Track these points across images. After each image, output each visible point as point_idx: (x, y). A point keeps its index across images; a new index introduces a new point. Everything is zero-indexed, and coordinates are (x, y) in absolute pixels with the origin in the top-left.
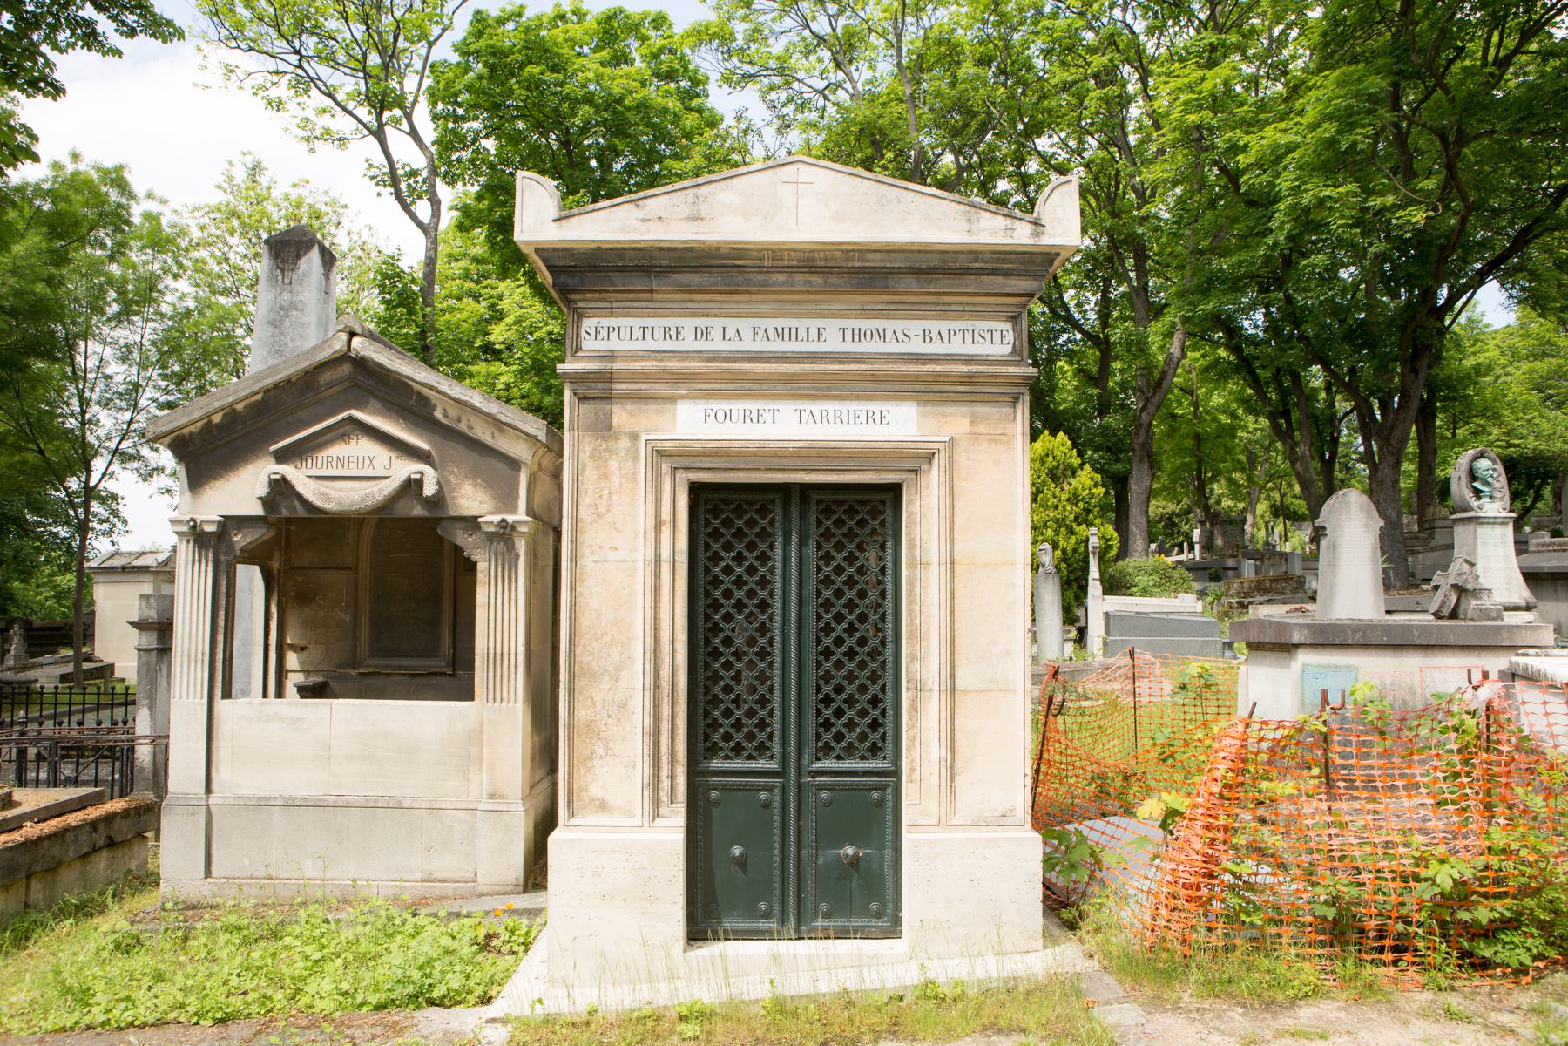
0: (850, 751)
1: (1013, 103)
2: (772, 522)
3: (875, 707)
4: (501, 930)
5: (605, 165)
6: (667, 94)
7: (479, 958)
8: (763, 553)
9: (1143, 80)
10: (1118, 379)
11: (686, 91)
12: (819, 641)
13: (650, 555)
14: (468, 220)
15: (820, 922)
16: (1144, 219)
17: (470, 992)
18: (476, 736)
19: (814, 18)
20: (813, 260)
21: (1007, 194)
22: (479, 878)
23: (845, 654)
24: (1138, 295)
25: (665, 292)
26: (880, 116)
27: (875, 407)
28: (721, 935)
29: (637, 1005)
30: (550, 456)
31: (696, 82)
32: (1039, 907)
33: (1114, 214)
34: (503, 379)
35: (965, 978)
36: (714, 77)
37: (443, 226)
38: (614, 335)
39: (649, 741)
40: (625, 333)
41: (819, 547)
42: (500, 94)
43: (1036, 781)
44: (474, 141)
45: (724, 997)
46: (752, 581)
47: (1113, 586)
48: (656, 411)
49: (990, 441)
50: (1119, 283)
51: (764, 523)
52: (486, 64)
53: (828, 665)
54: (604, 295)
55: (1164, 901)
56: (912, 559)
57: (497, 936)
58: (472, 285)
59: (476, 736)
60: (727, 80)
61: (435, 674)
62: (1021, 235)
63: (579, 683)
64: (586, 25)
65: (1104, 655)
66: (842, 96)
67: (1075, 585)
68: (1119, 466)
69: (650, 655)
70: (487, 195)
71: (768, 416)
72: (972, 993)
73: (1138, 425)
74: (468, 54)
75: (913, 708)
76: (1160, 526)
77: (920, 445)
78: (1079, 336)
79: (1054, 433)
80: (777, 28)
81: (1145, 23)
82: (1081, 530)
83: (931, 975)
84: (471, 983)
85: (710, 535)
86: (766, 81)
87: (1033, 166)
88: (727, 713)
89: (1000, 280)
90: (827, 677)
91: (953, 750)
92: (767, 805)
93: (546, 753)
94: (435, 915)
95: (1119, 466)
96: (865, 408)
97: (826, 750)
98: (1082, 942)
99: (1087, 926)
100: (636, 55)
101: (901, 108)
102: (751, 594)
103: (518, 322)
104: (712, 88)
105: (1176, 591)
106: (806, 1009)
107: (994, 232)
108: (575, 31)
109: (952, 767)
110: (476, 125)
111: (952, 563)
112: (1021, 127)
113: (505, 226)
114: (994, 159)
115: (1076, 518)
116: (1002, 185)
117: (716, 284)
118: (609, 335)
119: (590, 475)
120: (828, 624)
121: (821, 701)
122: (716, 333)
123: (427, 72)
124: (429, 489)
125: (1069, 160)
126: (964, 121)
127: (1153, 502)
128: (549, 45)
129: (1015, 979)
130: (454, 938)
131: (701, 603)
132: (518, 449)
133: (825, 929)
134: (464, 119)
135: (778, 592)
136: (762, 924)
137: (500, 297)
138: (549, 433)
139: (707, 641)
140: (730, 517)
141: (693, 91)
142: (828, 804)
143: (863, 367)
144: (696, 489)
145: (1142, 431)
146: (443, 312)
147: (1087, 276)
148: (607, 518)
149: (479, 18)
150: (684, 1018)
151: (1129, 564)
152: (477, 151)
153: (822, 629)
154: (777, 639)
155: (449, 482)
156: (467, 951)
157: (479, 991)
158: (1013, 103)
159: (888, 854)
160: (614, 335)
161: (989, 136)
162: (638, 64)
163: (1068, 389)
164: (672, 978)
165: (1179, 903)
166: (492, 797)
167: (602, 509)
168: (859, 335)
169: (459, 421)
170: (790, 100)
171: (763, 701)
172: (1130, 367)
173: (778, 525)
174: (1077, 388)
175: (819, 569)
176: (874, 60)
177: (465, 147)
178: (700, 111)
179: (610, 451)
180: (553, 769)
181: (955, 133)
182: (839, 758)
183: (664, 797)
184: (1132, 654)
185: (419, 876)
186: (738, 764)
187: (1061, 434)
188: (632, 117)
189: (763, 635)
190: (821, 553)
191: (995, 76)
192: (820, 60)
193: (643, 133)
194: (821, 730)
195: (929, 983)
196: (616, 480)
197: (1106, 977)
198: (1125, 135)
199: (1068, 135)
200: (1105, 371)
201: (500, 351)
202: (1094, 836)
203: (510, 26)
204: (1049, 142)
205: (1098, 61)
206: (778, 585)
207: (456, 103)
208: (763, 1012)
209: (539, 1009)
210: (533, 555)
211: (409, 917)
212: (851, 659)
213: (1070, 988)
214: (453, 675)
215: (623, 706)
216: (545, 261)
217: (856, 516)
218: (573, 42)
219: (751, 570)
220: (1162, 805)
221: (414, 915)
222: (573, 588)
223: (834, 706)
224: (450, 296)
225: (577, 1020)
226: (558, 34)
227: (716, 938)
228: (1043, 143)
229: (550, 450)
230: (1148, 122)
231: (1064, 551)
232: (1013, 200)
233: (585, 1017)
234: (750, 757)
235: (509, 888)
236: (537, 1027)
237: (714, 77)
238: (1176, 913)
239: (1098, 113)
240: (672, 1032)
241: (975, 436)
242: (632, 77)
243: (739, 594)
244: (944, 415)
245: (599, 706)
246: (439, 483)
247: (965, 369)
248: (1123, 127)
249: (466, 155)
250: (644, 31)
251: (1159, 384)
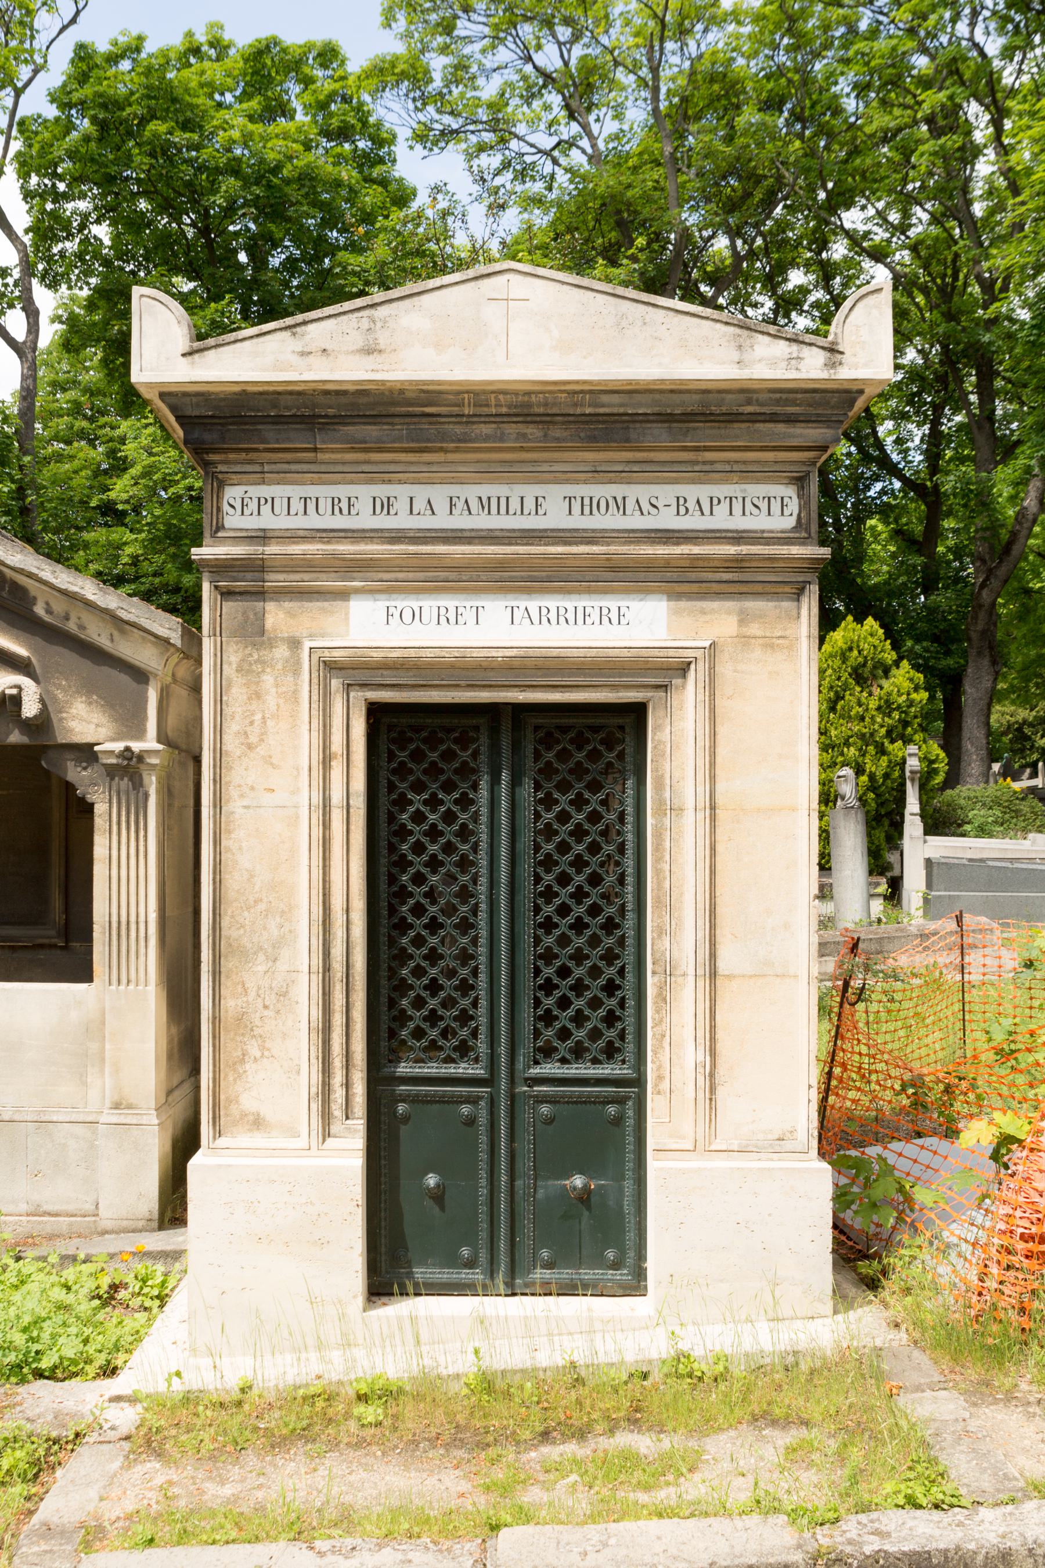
0: (578, 1053)
1: (814, 163)
2: (475, 755)
3: (611, 995)
4: (129, 1279)
5: (259, 260)
6: (339, 160)
7: (101, 1316)
8: (464, 795)
9: (997, 123)
10: (951, 543)
11: (365, 155)
12: (537, 910)
13: (317, 799)
14: (72, 343)
15: (539, 1274)
16: (994, 322)
17: (88, 1361)
18: (96, 1028)
19: (539, 47)
20: (530, 405)
21: (804, 291)
22: (103, 1212)
23: (571, 927)
24: (980, 428)
25: (333, 451)
26: (629, 186)
27: (612, 603)
28: (411, 1290)
29: (301, 1380)
30: (186, 664)
31: (379, 142)
32: (827, 1259)
33: (951, 316)
34: (129, 550)
35: (728, 1351)
36: (403, 134)
37: (45, 340)
38: (266, 509)
39: (317, 1040)
40: (280, 506)
41: (538, 787)
42: (115, 162)
43: (826, 1091)
44: (82, 227)
45: (415, 1370)
46: (449, 832)
47: (938, 823)
48: (323, 609)
49: (765, 646)
50: (956, 411)
51: (465, 755)
52: (94, 120)
53: (549, 941)
54: (252, 456)
55: (996, 1257)
56: (660, 802)
57: (125, 1286)
58: (85, 424)
59: (96, 1028)
60: (421, 137)
61: (42, 946)
62: (812, 367)
63: (228, 964)
64: (228, 63)
65: (926, 914)
66: (577, 158)
67: (886, 822)
68: (950, 662)
69: (317, 929)
70: (102, 303)
71: (469, 616)
72: (738, 1371)
73: (977, 606)
74: (70, 105)
75: (661, 998)
76: (1006, 739)
77: (671, 653)
78: (897, 485)
79: (860, 620)
80: (489, 62)
81: (1002, 41)
82: (896, 748)
83: (684, 1346)
84: (91, 1349)
85: (394, 772)
86: (473, 139)
87: (839, 250)
88: (419, 1003)
89: (781, 428)
90: (548, 957)
91: (713, 1053)
92: (471, 1121)
93: (185, 1051)
94: (44, 1259)
95: (950, 662)
96: (597, 604)
97: (547, 1052)
98: (886, 1305)
99: (891, 1285)
100: (296, 104)
101: (657, 173)
102: (449, 848)
103: (147, 473)
104: (400, 149)
105: (1025, 830)
106: (521, 1388)
107: (773, 364)
108: (214, 71)
109: (712, 1075)
110: (83, 205)
111: (713, 808)
112: (822, 195)
113: (120, 348)
114: (786, 241)
115: (889, 733)
116: (797, 278)
117: (400, 439)
118: (257, 509)
119: (237, 694)
120: (549, 887)
121: (541, 987)
122: (401, 506)
123: (14, 132)
124: (30, 709)
125: (889, 241)
126: (743, 193)
127: (998, 707)
128: (179, 92)
129: (795, 1353)
130: (69, 1288)
131: (383, 861)
132: (145, 656)
133: (546, 1283)
134: (66, 197)
135: (484, 845)
136: (465, 1275)
137: (123, 440)
138: (186, 634)
139: (392, 910)
140: (424, 748)
141: (374, 160)
142: (550, 1121)
143: (595, 549)
144: (375, 712)
145: (982, 615)
146: (47, 460)
147: (910, 403)
148: (261, 750)
149: (83, 54)
150: (362, 1398)
151: (961, 793)
152: (85, 241)
153: (541, 894)
154: (483, 906)
155: (55, 699)
156: (85, 1307)
157: (101, 1360)
158: (814, 163)
159: (628, 1186)
160: (266, 509)
161: (779, 210)
162: (300, 117)
163: (881, 554)
164: (347, 1344)
165: (1014, 1259)
166: (117, 1106)
167: (253, 739)
168: (590, 506)
169: (67, 618)
170: (506, 165)
171: (465, 987)
172: (966, 528)
173: (483, 758)
174: (894, 556)
175: (537, 816)
176: (621, 105)
177: (70, 236)
178: (383, 182)
179: (263, 662)
180: (195, 1071)
181: (731, 206)
182: (564, 1061)
183: (337, 1111)
184: (959, 919)
185: (23, 1207)
186: (432, 1069)
187: (870, 621)
188: (293, 193)
189: (464, 902)
190: (540, 795)
191: (788, 124)
192: (547, 108)
193: (308, 216)
194: (540, 1025)
195: (681, 1357)
196: (271, 701)
197: (916, 1353)
198: (969, 203)
199: (889, 205)
200: (933, 532)
201: (124, 513)
202: (903, 1164)
203: (125, 65)
204: (862, 215)
205: (932, 99)
206: (484, 837)
207: (55, 175)
208: (465, 1391)
209: (177, 1385)
210: (168, 793)
211: (11, 1262)
212: (579, 933)
213: (866, 1368)
214: (65, 948)
215: (283, 994)
216: (173, 409)
217: (586, 746)
218: (211, 88)
219: (449, 817)
220: (995, 1130)
221: (18, 1259)
222: (217, 842)
223: (557, 994)
224: (56, 438)
225: (227, 1399)
226: (190, 76)
227: (404, 1293)
228: (853, 218)
229: (187, 657)
230: (1001, 182)
231: (872, 777)
232: (811, 299)
233: (236, 1395)
234: (449, 1060)
235: (140, 1224)
236: (174, 1407)
237: (403, 134)
238: (1012, 1273)
239: (931, 174)
240: (348, 1416)
241: (745, 641)
242: (292, 137)
243: (433, 848)
244: (703, 612)
245: (252, 995)
246: (42, 700)
247: (731, 550)
248: (965, 190)
249: (71, 246)
250: (307, 70)
251: (1007, 549)
